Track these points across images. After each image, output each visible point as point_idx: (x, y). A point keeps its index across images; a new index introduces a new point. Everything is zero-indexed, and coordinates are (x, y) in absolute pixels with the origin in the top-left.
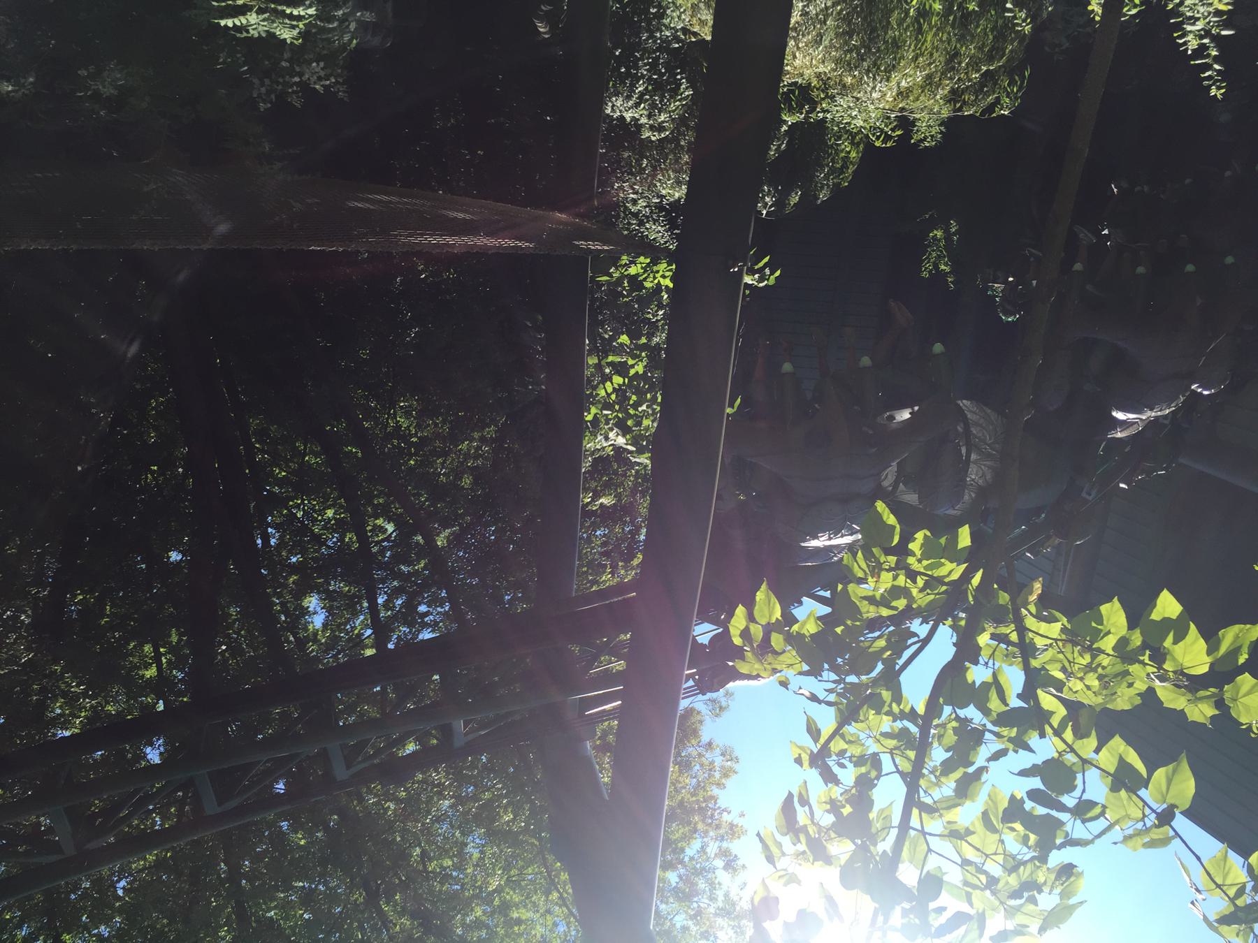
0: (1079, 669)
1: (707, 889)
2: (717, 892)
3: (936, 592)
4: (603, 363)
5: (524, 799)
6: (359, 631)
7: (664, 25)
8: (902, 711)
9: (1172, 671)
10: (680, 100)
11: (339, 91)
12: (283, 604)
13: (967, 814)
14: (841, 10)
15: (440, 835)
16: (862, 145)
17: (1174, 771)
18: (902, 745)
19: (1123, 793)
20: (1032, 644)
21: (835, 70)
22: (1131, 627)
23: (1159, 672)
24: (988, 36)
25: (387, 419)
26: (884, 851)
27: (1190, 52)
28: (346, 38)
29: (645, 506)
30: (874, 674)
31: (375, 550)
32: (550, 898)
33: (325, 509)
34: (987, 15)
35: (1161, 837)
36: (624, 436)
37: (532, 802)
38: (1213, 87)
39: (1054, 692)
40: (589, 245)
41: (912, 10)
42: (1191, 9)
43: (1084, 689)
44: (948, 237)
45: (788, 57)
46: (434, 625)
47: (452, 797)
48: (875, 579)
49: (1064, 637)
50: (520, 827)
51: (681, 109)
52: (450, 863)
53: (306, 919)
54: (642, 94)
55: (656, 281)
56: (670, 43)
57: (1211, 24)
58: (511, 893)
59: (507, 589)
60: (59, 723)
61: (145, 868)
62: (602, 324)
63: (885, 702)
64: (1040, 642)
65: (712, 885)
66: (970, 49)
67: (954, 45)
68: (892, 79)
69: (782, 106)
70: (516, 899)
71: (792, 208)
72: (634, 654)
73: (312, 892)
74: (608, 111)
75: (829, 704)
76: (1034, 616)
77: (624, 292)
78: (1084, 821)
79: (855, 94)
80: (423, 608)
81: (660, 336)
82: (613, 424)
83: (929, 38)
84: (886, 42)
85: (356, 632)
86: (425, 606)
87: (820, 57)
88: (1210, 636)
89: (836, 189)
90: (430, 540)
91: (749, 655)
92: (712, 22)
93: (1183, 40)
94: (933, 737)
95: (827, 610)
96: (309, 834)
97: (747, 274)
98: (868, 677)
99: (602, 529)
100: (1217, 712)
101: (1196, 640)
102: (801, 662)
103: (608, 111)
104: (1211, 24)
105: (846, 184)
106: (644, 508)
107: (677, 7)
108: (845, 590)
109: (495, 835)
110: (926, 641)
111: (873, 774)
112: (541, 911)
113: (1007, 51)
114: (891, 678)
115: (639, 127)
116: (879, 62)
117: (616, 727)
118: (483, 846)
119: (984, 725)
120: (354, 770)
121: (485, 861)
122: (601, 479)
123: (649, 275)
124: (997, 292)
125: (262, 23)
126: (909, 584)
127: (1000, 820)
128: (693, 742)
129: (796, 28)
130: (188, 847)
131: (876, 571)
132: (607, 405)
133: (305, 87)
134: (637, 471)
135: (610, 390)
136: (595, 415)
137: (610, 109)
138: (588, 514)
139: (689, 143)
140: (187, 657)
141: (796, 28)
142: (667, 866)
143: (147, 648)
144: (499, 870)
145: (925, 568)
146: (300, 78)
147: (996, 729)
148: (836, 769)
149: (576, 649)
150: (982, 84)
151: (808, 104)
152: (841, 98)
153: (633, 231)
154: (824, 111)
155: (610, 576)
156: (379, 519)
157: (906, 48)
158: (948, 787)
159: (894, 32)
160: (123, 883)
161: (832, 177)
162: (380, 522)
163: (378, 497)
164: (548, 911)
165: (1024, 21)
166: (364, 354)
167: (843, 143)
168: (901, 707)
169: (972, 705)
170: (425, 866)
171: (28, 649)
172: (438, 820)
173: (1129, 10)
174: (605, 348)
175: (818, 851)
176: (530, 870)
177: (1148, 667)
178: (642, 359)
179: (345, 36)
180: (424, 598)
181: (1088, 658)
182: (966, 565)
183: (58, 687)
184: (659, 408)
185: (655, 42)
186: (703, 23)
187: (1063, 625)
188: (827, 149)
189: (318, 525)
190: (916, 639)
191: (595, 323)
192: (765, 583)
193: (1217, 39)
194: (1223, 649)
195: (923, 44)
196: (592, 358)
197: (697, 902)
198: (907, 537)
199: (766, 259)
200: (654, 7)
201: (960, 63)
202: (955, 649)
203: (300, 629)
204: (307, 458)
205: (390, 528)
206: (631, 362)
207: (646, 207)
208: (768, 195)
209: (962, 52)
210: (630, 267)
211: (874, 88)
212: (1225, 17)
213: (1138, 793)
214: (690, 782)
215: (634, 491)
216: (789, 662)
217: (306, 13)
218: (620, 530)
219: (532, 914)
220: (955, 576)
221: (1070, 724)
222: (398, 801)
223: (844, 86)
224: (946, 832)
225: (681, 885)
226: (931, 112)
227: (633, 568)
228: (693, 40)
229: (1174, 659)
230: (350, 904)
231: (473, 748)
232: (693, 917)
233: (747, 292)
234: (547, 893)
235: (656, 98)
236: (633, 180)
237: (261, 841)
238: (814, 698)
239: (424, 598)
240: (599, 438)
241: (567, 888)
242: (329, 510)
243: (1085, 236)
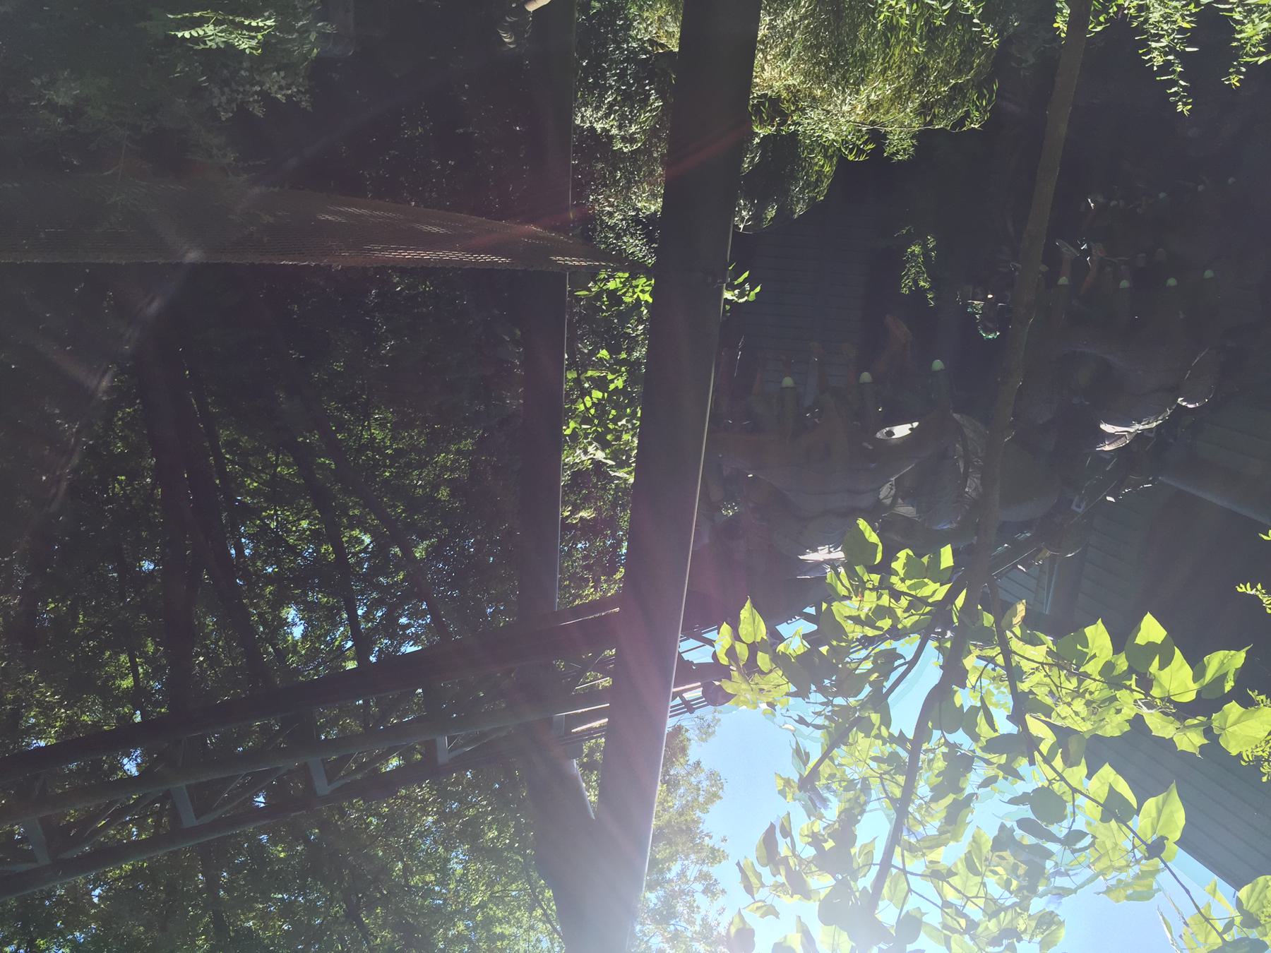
0: (1066, 693)
1: (685, 912)
2: (696, 916)
3: (921, 612)
4: (582, 377)
6: (340, 643)
7: (631, 36)
8: (891, 735)
9: (1159, 698)
10: (650, 111)
11: (301, 101)
12: (260, 615)
14: (809, 24)
15: (423, 850)
16: (835, 158)
17: (1164, 803)
18: (892, 770)
19: (1113, 823)
20: (1019, 667)
21: (804, 83)
22: (1117, 650)
23: (1146, 698)
24: (955, 50)
25: (361, 431)
27: (1155, 69)
28: (306, 47)
29: (626, 519)
30: (862, 696)
31: (352, 561)
32: (534, 915)
33: (299, 520)
34: (954, 30)
35: (1151, 869)
36: (603, 450)
37: (518, 820)
38: (1180, 103)
39: (1043, 718)
40: (566, 260)
41: (879, 25)
42: (1156, 26)
43: (1074, 716)
44: (926, 253)
45: (757, 69)
46: (416, 639)
47: (436, 813)
48: (859, 599)
49: (1050, 660)
50: (505, 844)
51: (652, 120)
52: (433, 878)
53: (285, 930)
54: (611, 105)
55: (635, 296)
56: (637, 54)
57: (1176, 41)
58: (494, 908)
59: (489, 601)
60: (34, 733)
62: (581, 339)
63: (874, 725)
64: (1026, 666)
65: (692, 908)
66: (938, 63)
67: (922, 59)
69: (754, 118)
70: (500, 914)
71: (769, 221)
72: (618, 670)
73: (291, 903)
74: (578, 122)
75: (817, 727)
77: (603, 307)
78: (1074, 851)
80: (403, 620)
81: (640, 351)
82: (592, 438)
83: (897, 52)
84: (854, 56)
85: (337, 643)
86: (406, 619)
87: (788, 69)
88: (1195, 661)
90: (407, 551)
91: (735, 674)
92: (679, 34)
93: (1149, 57)
94: (923, 762)
95: (814, 627)
96: (290, 848)
97: (727, 290)
98: (857, 699)
99: (583, 542)
100: (1206, 742)
101: (1181, 667)
102: (788, 683)
103: (578, 122)
104: (1176, 41)
105: (822, 198)
106: (625, 521)
109: (479, 852)
110: (912, 664)
112: (524, 927)
113: (975, 65)
114: (879, 701)
116: (848, 75)
117: (603, 745)
119: (974, 751)
120: (337, 785)
121: (467, 877)
122: (580, 492)
123: (628, 289)
124: (977, 310)
125: (220, 34)
126: (893, 604)
128: (682, 760)
129: (764, 41)
130: (166, 858)
131: (860, 590)
132: (586, 419)
133: (266, 97)
134: (617, 485)
135: (589, 404)
136: (574, 429)
138: (567, 527)
140: (164, 667)
141: (764, 41)
142: (651, 888)
143: (123, 658)
144: (482, 886)
145: (909, 588)
146: (261, 86)
147: (987, 756)
149: (562, 665)
150: (951, 98)
151: (779, 116)
152: (812, 111)
153: (610, 244)
154: (795, 124)
155: (592, 590)
156: (355, 530)
157: (874, 61)
159: (861, 46)
160: (97, 892)
161: (807, 191)
162: (356, 533)
163: (353, 507)
164: (532, 928)
165: (991, 35)
166: (339, 366)
167: (816, 156)
170: (407, 881)
172: (421, 835)
173: (1094, 28)
174: (582, 364)
175: (797, 886)
176: (514, 886)
177: (1135, 693)
178: (622, 375)
179: (305, 46)
180: (404, 610)
181: (1074, 681)
182: (949, 585)
183: (33, 697)
184: (638, 423)
185: (622, 53)
186: (670, 35)
187: (1048, 647)
188: (800, 162)
189: (293, 535)
190: (902, 661)
191: (574, 339)
192: (749, 601)
193: (1182, 56)
194: (1210, 675)
195: (890, 58)
197: (674, 925)
198: (890, 555)
199: (746, 275)
200: (620, 20)
201: (928, 76)
203: (279, 640)
204: (279, 469)
205: (367, 539)
206: (610, 377)
207: (622, 220)
208: (744, 210)
209: (930, 66)
210: (609, 282)
211: (844, 101)
212: (1189, 34)
213: (1128, 823)
214: (676, 803)
215: (614, 505)
216: (776, 682)
217: (265, 25)
218: (602, 544)
219: (516, 930)
220: (939, 596)
221: (1060, 751)
222: (379, 816)
224: (928, 872)
226: (902, 125)
227: (615, 582)
228: (661, 51)
229: (1161, 686)
230: (330, 916)
231: (461, 763)
232: (668, 941)
233: (728, 307)
234: (531, 909)
235: (626, 109)
236: (608, 192)
237: (239, 854)
238: (801, 721)
239: (404, 610)
240: (578, 452)
241: (551, 905)
242: (304, 521)
243: (1067, 251)
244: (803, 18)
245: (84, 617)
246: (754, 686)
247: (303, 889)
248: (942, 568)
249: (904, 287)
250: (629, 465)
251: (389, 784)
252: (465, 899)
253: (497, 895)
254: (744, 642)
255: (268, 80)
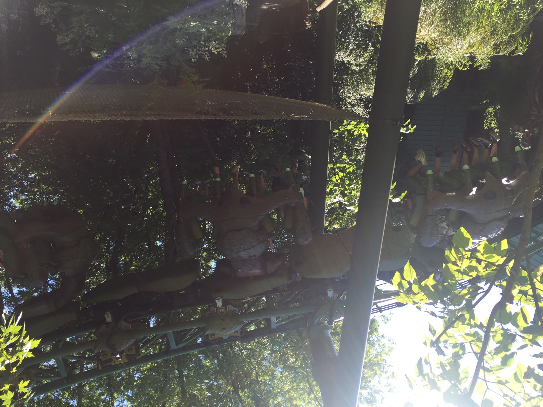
3: (491, 269)
5: (300, 353)
8: (475, 324)
11: (223, 54)
13: (507, 373)
14: (442, 10)
18: (475, 340)
25: (243, 190)
26: (465, 388)
55: (359, 132)
58: (293, 393)
61: (146, 370)
63: (466, 319)
68: (466, 39)
70: (295, 396)
74: (337, 58)
75: (441, 317)
76: (540, 282)
79: (449, 47)
87: (432, 30)
89: (442, 91)
103: (337, 58)
105: (446, 88)
107: (367, 12)
108: (447, 267)
110: (487, 292)
111: (461, 352)
112: (306, 402)
114: (470, 307)
115: (351, 64)
118: (282, 372)
119: (516, 332)
122: (332, 216)
126: (478, 265)
127: (523, 377)
131: (461, 258)
132: (336, 185)
133: (210, 53)
134: (348, 214)
135: (338, 178)
137: (337, 57)
139: (373, 71)
145: (485, 258)
147: (522, 335)
148: (443, 349)
154: (434, 54)
158: (498, 359)
160: (137, 375)
164: (309, 402)
168: (475, 321)
169: (510, 323)
170: (257, 378)
171: (104, 278)
172: (263, 359)
174: (339, 160)
190: (482, 290)
196: (331, 165)
199: (409, 121)
202: (501, 296)
222: (247, 349)
223: (443, 43)
224: (496, 381)
225: (369, 397)
228: (374, 25)
231: (280, 329)
234: (309, 395)
237: (192, 362)
238: (433, 314)
244: (439, 8)
245: (135, 263)
246: (411, 300)
247: (216, 380)
248: (502, 250)
249: (486, 126)
250: (355, 205)
251: (250, 336)
252: (281, 387)
253: (295, 387)
254: (406, 280)
255: (211, 45)
